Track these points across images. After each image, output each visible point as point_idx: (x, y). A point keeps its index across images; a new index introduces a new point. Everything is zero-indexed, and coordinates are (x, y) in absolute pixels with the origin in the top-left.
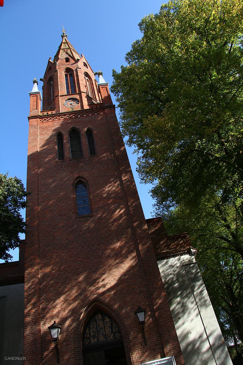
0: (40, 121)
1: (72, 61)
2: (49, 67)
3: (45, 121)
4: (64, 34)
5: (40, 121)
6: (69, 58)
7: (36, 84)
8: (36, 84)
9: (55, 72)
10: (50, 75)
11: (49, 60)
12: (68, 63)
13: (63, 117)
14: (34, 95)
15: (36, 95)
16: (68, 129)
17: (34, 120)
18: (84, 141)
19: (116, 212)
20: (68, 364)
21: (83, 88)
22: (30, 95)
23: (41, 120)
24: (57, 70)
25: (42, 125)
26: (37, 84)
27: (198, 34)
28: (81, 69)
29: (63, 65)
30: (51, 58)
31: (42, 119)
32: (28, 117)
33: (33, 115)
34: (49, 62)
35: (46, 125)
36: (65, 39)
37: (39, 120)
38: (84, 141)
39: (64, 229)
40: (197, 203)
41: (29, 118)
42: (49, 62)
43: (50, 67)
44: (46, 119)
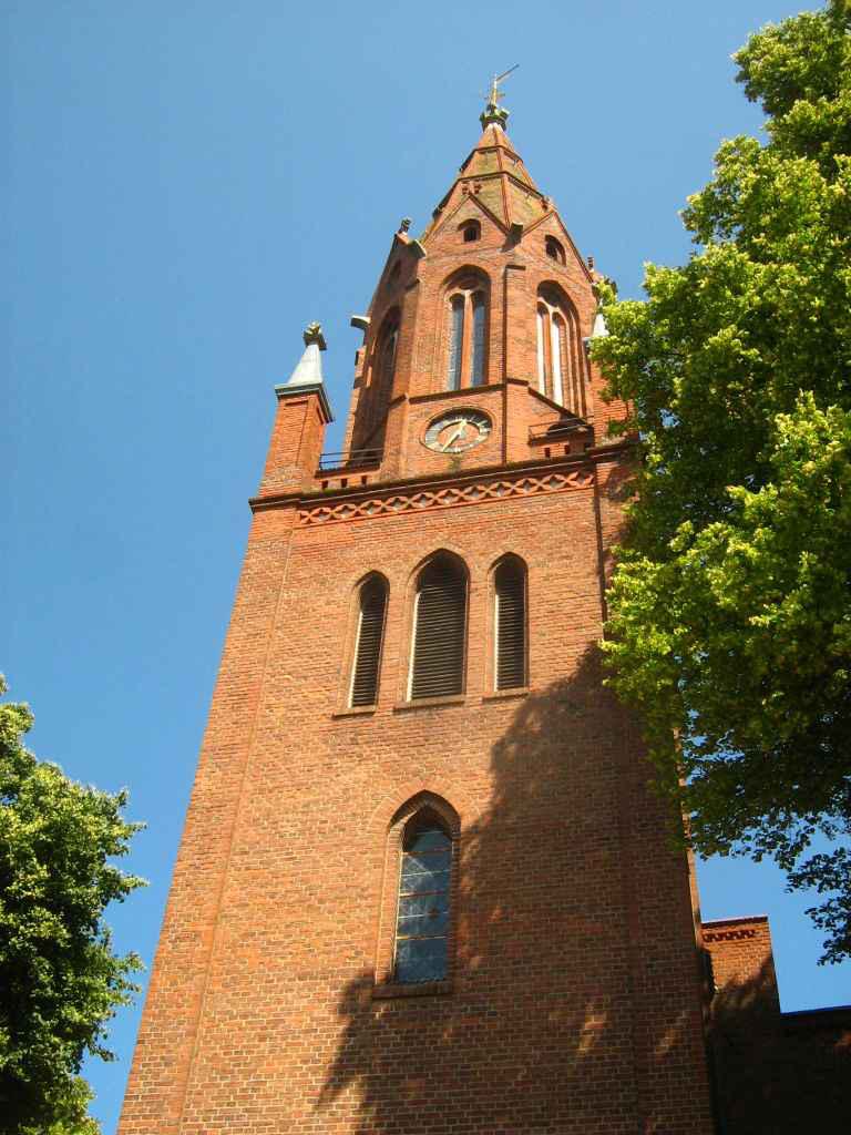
0: (302, 517)
1: (492, 235)
2: (393, 264)
3: (320, 520)
4: (491, 108)
5: (302, 517)
6: (484, 220)
7: (314, 348)
8: (314, 348)
9: (408, 288)
10: (392, 304)
11: (400, 232)
12: (472, 245)
13: (403, 503)
14: (296, 400)
15: (304, 398)
16: (416, 560)
17: (275, 513)
18: (485, 612)
19: (736, 486)
20: (451, 1133)
21: (517, 358)
22: (280, 398)
23: (305, 513)
24: (418, 281)
25: (302, 538)
26: (323, 347)
27: (679, 377)
28: (523, 268)
29: (448, 253)
30: (407, 222)
31: (310, 511)
32: (251, 503)
33: (274, 492)
34: (397, 241)
35: (323, 534)
36: (494, 130)
37: (290, 512)
38: (485, 612)
39: (310, 1044)
40: (827, 388)
41: (258, 505)
42: (397, 241)
43: (398, 264)
44: (325, 509)
